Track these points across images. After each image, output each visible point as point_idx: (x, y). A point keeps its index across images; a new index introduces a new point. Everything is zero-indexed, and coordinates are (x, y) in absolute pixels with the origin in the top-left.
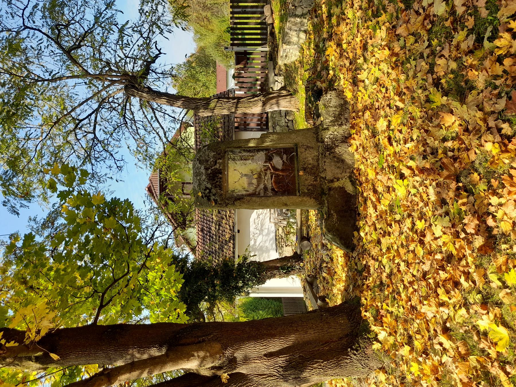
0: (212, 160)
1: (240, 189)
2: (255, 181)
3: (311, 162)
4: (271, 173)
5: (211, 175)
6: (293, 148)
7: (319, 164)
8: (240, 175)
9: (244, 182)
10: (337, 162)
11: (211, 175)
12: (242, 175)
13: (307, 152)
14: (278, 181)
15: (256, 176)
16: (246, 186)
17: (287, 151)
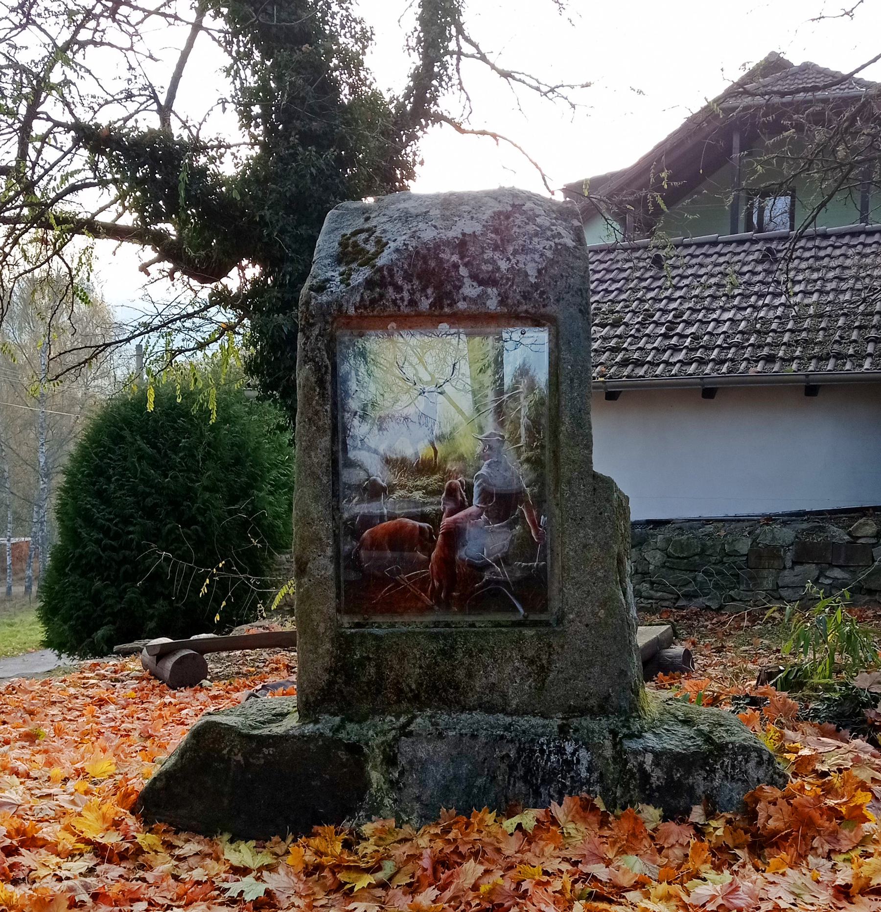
0: (503, 265)
4: (439, 515)
7: (471, 710)
11: (432, 264)
17: (533, 589)
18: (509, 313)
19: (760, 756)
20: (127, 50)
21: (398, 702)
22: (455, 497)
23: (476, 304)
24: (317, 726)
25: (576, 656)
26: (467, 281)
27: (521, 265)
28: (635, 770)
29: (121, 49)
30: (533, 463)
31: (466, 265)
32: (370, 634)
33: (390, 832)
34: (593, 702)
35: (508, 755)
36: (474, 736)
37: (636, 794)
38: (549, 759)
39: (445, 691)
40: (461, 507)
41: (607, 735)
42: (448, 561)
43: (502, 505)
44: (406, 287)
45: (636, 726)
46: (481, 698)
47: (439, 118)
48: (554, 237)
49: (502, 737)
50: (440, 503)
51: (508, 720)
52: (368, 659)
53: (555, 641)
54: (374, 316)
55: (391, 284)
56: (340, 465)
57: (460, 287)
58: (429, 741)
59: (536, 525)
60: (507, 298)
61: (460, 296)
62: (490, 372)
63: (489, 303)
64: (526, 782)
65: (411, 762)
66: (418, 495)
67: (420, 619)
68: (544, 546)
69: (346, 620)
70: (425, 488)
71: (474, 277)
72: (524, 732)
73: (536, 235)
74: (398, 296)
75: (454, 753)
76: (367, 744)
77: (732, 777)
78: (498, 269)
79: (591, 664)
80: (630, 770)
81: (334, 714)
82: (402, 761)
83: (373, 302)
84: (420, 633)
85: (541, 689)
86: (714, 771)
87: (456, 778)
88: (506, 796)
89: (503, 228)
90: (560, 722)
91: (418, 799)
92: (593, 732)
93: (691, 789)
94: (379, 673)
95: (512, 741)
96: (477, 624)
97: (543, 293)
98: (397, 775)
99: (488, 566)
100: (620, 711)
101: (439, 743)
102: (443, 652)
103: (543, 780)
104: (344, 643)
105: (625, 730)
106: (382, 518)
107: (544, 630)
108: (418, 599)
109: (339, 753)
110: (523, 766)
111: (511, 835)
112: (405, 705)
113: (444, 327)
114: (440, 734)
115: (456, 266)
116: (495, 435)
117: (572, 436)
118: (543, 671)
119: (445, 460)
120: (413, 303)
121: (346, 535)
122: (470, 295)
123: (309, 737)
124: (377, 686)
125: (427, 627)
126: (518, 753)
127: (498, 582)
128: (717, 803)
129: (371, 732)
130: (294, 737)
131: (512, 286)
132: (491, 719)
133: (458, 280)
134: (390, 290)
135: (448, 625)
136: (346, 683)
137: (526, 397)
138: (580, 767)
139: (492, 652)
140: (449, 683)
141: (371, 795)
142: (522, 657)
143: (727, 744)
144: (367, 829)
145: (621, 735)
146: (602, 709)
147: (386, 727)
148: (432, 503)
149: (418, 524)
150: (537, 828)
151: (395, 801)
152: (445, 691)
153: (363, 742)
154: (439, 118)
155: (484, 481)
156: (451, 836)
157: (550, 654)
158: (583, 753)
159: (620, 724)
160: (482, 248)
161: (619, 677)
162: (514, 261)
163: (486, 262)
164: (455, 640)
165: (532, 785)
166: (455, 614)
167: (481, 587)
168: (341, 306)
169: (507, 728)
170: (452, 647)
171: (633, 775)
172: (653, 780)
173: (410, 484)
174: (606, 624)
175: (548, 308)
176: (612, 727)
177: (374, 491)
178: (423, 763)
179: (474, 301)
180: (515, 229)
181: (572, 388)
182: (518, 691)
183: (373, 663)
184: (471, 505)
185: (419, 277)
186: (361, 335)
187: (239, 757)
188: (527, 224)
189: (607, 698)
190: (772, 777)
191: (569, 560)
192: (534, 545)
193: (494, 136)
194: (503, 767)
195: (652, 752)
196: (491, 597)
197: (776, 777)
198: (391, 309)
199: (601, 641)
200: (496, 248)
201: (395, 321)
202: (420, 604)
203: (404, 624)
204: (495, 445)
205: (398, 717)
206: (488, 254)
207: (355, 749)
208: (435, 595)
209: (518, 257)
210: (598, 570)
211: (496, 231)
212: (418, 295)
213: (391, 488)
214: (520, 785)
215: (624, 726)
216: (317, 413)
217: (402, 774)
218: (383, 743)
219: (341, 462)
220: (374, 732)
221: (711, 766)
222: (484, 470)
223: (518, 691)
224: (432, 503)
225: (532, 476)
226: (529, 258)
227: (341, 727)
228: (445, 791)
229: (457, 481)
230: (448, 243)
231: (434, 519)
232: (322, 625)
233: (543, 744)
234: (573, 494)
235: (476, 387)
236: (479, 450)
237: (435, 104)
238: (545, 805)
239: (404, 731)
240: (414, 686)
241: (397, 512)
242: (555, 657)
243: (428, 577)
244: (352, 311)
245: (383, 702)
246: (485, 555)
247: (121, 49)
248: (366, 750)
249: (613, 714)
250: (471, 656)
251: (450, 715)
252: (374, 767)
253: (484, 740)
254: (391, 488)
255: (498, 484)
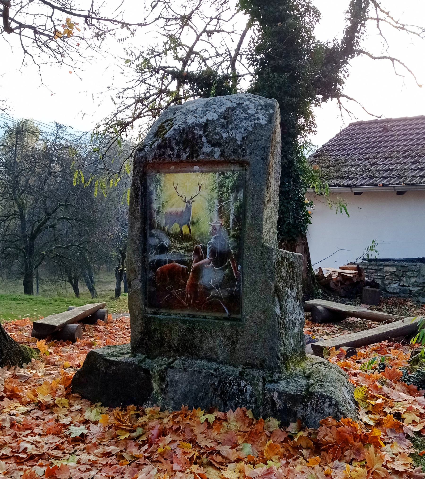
0: (225, 136)
1: (162, 200)
2: (176, 228)
3: (205, 346)
4: (191, 261)
5: (190, 136)
6: (238, 312)
7: (202, 359)
8: (188, 199)
9: (176, 206)
10: (196, 396)
11: (190, 136)
12: (189, 203)
13: (225, 342)
14: (175, 275)
15: (185, 230)
16: (169, 209)
17: (234, 301)
18: (225, 160)
19: (331, 401)
20: (231, 33)
21: (170, 351)
22: (199, 253)
23: (209, 156)
24: (134, 359)
25: (250, 338)
26: (206, 144)
27: (234, 135)
28: (269, 400)
29: (228, 33)
30: (235, 238)
31: (206, 136)
32: (157, 318)
33: (156, 413)
34: (257, 362)
35: (214, 384)
36: (200, 372)
37: (269, 411)
38: (232, 388)
39: (191, 348)
40: (201, 258)
41: (261, 379)
42: (194, 286)
43: (220, 258)
44: (176, 148)
45: (276, 377)
46: (206, 354)
47: (360, 52)
48: (255, 119)
49: (212, 374)
50: (192, 256)
51: (217, 366)
52: (157, 330)
53: (239, 329)
54: (161, 163)
55: (169, 147)
56: (148, 236)
57: (202, 147)
58: (180, 372)
59: (236, 270)
60: (224, 153)
61: (202, 152)
62: (216, 191)
63: (215, 155)
64: (221, 398)
65: (171, 381)
66: (182, 251)
67: (181, 312)
68: (239, 281)
69: (149, 310)
70: (185, 248)
71: (209, 142)
72: (223, 373)
73: (245, 119)
74: (172, 153)
75: (190, 379)
76: (152, 370)
77: (316, 410)
78: (222, 138)
79: (257, 343)
80: (267, 399)
81: (143, 354)
82: (168, 380)
83: (160, 156)
84: (178, 319)
85: (233, 352)
86: (307, 406)
87: (190, 391)
88: (211, 404)
89: (229, 116)
90: (241, 370)
91: (173, 399)
92: (255, 377)
93: (295, 413)
94: (161, 337)
95: (216, 377)
96: (207, 317)
97: (244, 149)
98: (164, 386)
99: (212, 288)
100: (270, 368)
101: (184, 374)
102: (188, 329)
103: (229, 398)
104: (147, 321)
105: (269, 378)
106: (165, 262)
107: (234, 323)
108: (180, 302)
109: (141, 373)
110: (221, 390)
111: (202, 423)
112: (172, 353)
113: (196, 168)
114: (185, 369)
115: (201, 137)
116: (218, 223)
117: (252, 225)
118: (234, 343)
119: (194, 234)
120: (178, 156)
121: (150, 270)
122: (206, 151)
123: (129, 363)
124: (161, 342)
125: (185, 317)
126: (219, 383)
127: (217, 297)
128: (308, 423)
129: (155, 365)
130: (123, 363)
131: (227, 146)
132: (209, 364)
133: (201, 144)
134: (169, 149)
135: (194, 316)
136: (149, 340)
137: (233, 204)
138: (246, 394)
139: (211, 331)
140: (192, 345)
141: (153, 394)
142: (224, 335)
143: (314, 392)
144: (148, 410)
145: (267, 380)
146: (262, 366)
147: (163, 363)
148: (188, 256)
149: (181, 266)
150: (214, 422)
151: (163, 398)
152: (191, 348)
153: (150, 369)
154: (360, 52)
155: (212, 246)
156: (177, 420)
157: (237, 335)
158: (249, 387)
159: (268, 375)
160: (216, 127)
161: (270, 350)
162: (230, 133)
163: (216, 134)
164: (194, 324)
165: (223, 400)
166: (197, 311)
167: (208, 300)
168: (146, 158)
169: (215, 370)
170: (193, 328)
171: (268, 402)
172: (277, 406)
173: (178, 246)
174: (265, 322)
175: (245, 158)
176: (264, 376)
177: (162, 249)
178: (176, 382)
179: (208, 155)
180: (235, 116)
181: (253, 199)
182: (222, 352)
183: (159, 332)
184: (205, 258)
185: (183, 143)
186: (159, 172)
187: (103, 369)
188: (242, 113)
189: (264, 360)
190: (336, 413)
191: (247, 288)
192: (234, 279)
193: (393, 60)
194: (212, 389)
195: (277, 391)
196: (213, 306)
197: (339, 413)
198: (168, 159)
199: (262, 331)
200: (223, 126)
201: (173, 165)
202: (181, 305)
203: (175, 314)
204: (218, 228)
205: (169, 359)
206: (218, 130)
207: (147, 371)
208: (188, 300)
209: (233, 131)
210: (262, 295)
211: (225, 118)
212: (181, 152)
213: (170, 248)
214: (218, 398)
215: (269, 376)
216: (134, 210)
217: (167, 386)
218: (159, 370)
219: (148, 234)
220: (156, 365)
221: (306, 403)
222: (212, 241)
223: (222, 352)
224: (188, 256)
225: (235, 244)
226: (238, 131)
227: (144, 360)
228: (185, 397)
229: (199, 246)
230: (199, 125)
231: (189, 264)
232: (137, 312)
233: (231, 380)
234: (251, 255)
235: (210, 198)
236: (210, 230)
237: (358, 45)
238: (225, 411)
239: (170, 366)
240: (176, 345)
241: (172, 259)
242: (239, 337)
243: (185, 292)
244: (151, 161)
245: (163, 350)
246: (211, 284)
247: (228, 33)
248: (151, 373)
249: (266, 369)
250: (201, 333)
251: (192, 360)
252: (155, 381)
253: (204, 374)
254: (170, 248)
255: (219, 247)
